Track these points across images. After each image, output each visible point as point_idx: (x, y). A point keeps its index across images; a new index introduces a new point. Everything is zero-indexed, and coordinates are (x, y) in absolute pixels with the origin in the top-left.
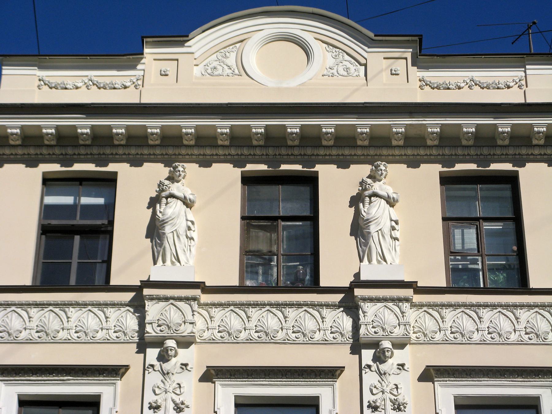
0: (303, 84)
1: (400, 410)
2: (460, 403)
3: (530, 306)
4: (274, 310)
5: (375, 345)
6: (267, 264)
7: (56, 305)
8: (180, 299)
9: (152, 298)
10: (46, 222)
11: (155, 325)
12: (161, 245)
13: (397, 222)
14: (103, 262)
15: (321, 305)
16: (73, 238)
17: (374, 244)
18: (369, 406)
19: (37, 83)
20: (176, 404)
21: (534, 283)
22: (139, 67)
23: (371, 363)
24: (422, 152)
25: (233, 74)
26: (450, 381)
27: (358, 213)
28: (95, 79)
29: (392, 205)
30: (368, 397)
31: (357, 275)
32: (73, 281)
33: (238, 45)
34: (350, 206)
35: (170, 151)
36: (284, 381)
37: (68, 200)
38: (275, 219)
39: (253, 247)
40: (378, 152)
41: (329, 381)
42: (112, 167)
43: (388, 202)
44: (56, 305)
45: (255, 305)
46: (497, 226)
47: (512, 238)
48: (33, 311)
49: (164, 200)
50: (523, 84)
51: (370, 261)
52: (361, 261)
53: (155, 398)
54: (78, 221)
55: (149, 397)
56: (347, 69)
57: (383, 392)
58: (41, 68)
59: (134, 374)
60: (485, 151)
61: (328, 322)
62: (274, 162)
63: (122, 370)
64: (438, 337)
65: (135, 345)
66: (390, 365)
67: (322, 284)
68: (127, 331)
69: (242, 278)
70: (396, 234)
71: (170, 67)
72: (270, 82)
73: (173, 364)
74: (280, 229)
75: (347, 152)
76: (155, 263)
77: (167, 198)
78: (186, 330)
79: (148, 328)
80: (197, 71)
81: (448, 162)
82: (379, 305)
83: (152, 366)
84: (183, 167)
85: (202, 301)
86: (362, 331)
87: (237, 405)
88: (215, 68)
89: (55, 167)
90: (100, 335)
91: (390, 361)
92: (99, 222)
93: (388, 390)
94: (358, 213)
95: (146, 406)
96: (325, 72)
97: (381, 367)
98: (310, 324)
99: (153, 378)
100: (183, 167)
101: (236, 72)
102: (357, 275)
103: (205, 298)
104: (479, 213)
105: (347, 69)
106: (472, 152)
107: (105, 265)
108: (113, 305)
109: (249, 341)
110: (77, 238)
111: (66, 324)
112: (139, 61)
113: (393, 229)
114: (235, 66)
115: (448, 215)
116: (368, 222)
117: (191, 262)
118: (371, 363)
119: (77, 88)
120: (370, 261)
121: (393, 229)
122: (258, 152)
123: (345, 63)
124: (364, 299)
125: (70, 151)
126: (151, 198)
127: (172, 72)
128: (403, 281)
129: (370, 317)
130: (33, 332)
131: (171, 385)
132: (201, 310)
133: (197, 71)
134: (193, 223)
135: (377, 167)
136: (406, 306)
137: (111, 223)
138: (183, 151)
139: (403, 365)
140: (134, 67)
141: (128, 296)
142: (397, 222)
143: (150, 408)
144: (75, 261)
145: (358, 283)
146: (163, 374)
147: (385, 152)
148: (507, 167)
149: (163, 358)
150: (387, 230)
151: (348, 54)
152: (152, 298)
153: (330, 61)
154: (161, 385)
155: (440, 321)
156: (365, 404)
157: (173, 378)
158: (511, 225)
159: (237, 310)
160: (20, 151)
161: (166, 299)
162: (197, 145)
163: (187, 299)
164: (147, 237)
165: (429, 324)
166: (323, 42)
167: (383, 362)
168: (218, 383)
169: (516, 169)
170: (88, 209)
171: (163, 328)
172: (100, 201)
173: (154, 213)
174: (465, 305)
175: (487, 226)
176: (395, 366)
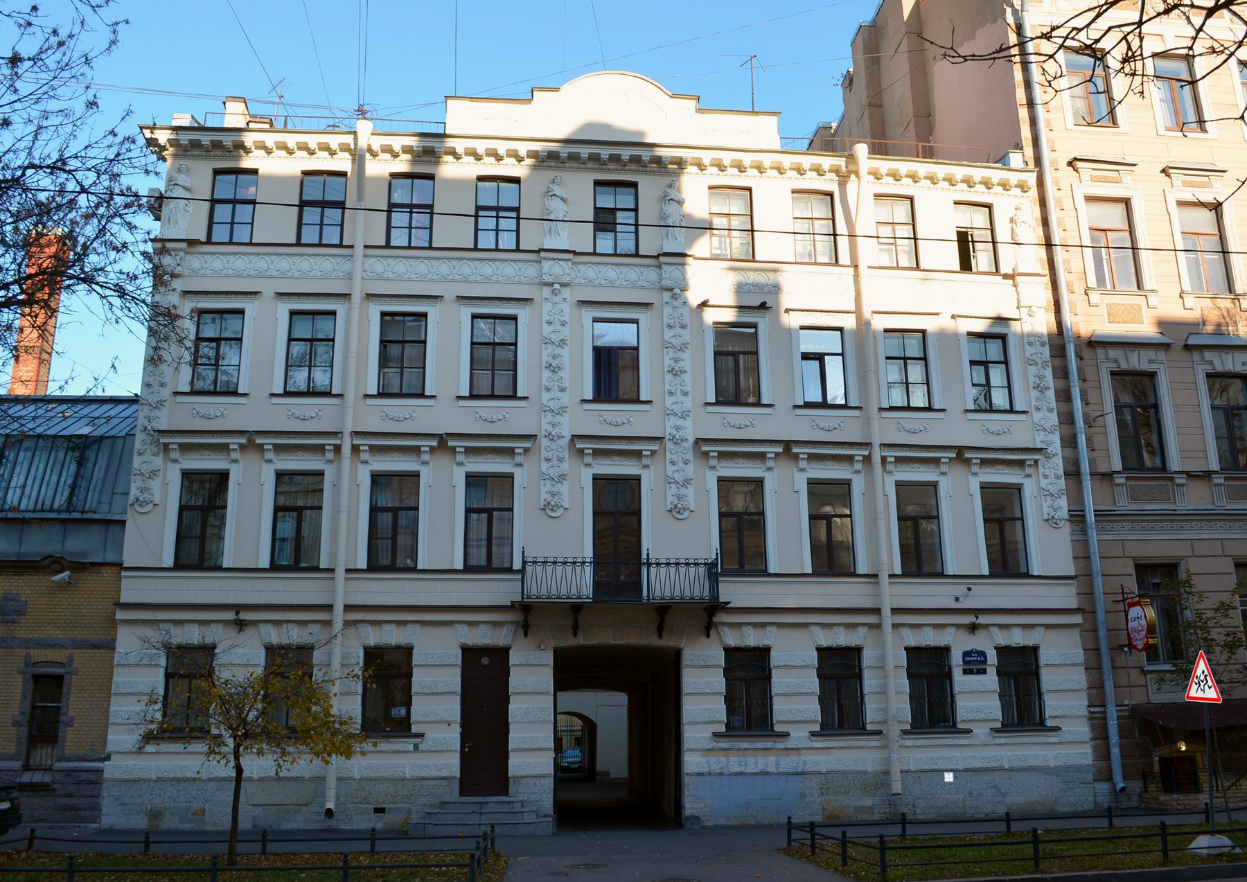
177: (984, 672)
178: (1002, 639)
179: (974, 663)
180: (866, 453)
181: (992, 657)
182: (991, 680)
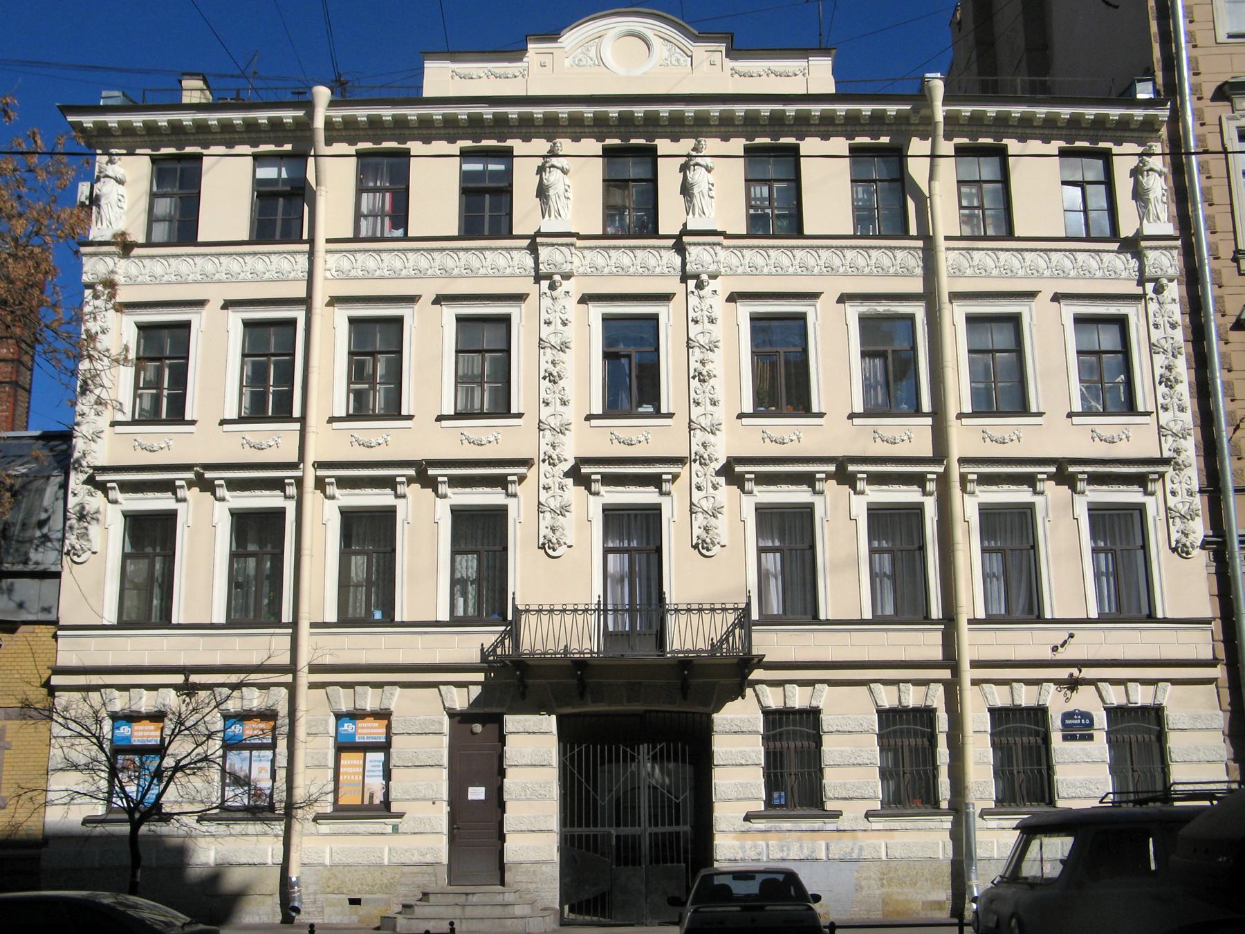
0: (645, 73)
1: (713, 323)
2: (605, 317)
3: (803, 248)
4: (627, 251)
5: (696, 277)
6: (622, 215)
7: (476, 249)
8: (562, 245)
9: (543, 245)
10: (465, 185)
11: (546, 264)
12: (547, 203)
13: (713, 185)
14: (507, 214)
15: (660, 248)
16: (278, 200)
17: (696, 201)
18: (692, 320)
19: (451, 74)
20: (562, 321)
21: (806, 232)
22: (525, 59)
23: (694, 290)
24: (731, 129)
25: (594, 64)
26: (747, 302)
27: (685, 178)
28: (493, 70)
29: (709, 172)
30: (691, 314)
31: (685, 225)
32: (486, 232)
33: (597, 40)
34: (680, 172)
35: (551, 130)
36: (635, 303)
37: (478, 167)
38: (627, 181)
39: (612, 202)
40: (700, 129)
41: (666, 303)
42: (509, 143)
43: (707, 170)
44: (476, 249)
45: (615, 248)
46: (784, 185)
47: (793, 193)
48: (461, 254)
49: (548, 169)
50: (806, 73)
51: (694, 214)
52: (688, 214)
53: (549, 316)
54: (487, 184)
55: (544, 316)
56: (678, 60)
57: (702, 310)
58: (453, 61)
59: (679, 299)
60: (777, 128)
61: (665, 260)
62: (625, 138)
63: (417, 298)
64: (740, 270)
65: (533, 278)
66: (707, 291)
67: (660, 233)
68: (527, 268)
69: (855, 229)
70: (712, 194)
71: (547, 59)
72: (621, 71)
73: (559, 292)
74: (631, 187)
75: (677, 129)
76: (543, 217)
77: (550, 168)
78: (567, 268)
79: (541, 266)
80: (567, 62)
81: (750, 137)
82: (700, 248)
83: (545, 293)
84: (560, 143)
85: (577, 246)
86: (688, 267)
87: (603, 319)
88: (581, 60)
89: (468, 143)
90: (508, 271)
91: (707, 288)
92: (502, 185)
93: (705, 309)
94: (685, 178)
95: (542, 322)
96: (662, 63)
97: (554, 293)
98: (652, 261)
99: (546, 302)
100: (560, 143)
101: (597, 63)
102: (685, 225)
103: (579, 243)
104: (771, 175)
105: (678, 60)
106: (767, 129)
107: (508, 217)
108: (516, 249)
109: (611, 274)
110: (487, 196)
111: (484, 263)
112: (524, 55)
113: (710, 190)
114: (595, 58)
115: (749, 177)
116: (548, 187)
117: (569, 217)
118: (694, 290)
119: (515, 77)
120: (694, 214)
121: (710, 190)
122: (614, 130)
123: (676, 55)
124: (690, 244)
125: (478, 131)
126: (539, 167)
127: (549, 64)
128: (716, 230)
129: (693, 258)
130: (462, 269)
131: (558, 307)
132: (577, 252)
133: (567, 62)
134: (569, 186)
135: (699, 142)
136: (718, 248)
137: (511, 185)
138: (560, 130)
139: (715, 291)
140: (520, 60)
141: (526, 242)
142: (713, 185)
143: (545, 323)
144: (487, 214)
145: (685, 232)
146: (553, 299)
147: (705, 129)
148: (792, 140)
149: (552, 287)
150: (561, 193)
151: (679, 48)
152: (543, 245)
153: (666, 54)
154: (552, 307)
155: (741, 258)
156: (690, 319)
157: (560, 301)
158: (793, 185)
159: (602, 251)
160: (442, 131)
161: (553, 245)
162: (569, 126)
163: (567, 245)
164: (537, 197)
165: (734, 261)
166: (660, 37)
167: (702, 289)
168: (590, 304)
169: (798, 142)
170: (495, 174)
171: (551, 266)
172: (502, 167)
173: (541, 180)
174: (758, 247)
175: (776, 185)
176: (711, 292)
177: (1091, 738)
178: (1115, 696)
179: (1078, 727)
180: (940, 469)
181: (1101, 719)
182: (1099, 746)
